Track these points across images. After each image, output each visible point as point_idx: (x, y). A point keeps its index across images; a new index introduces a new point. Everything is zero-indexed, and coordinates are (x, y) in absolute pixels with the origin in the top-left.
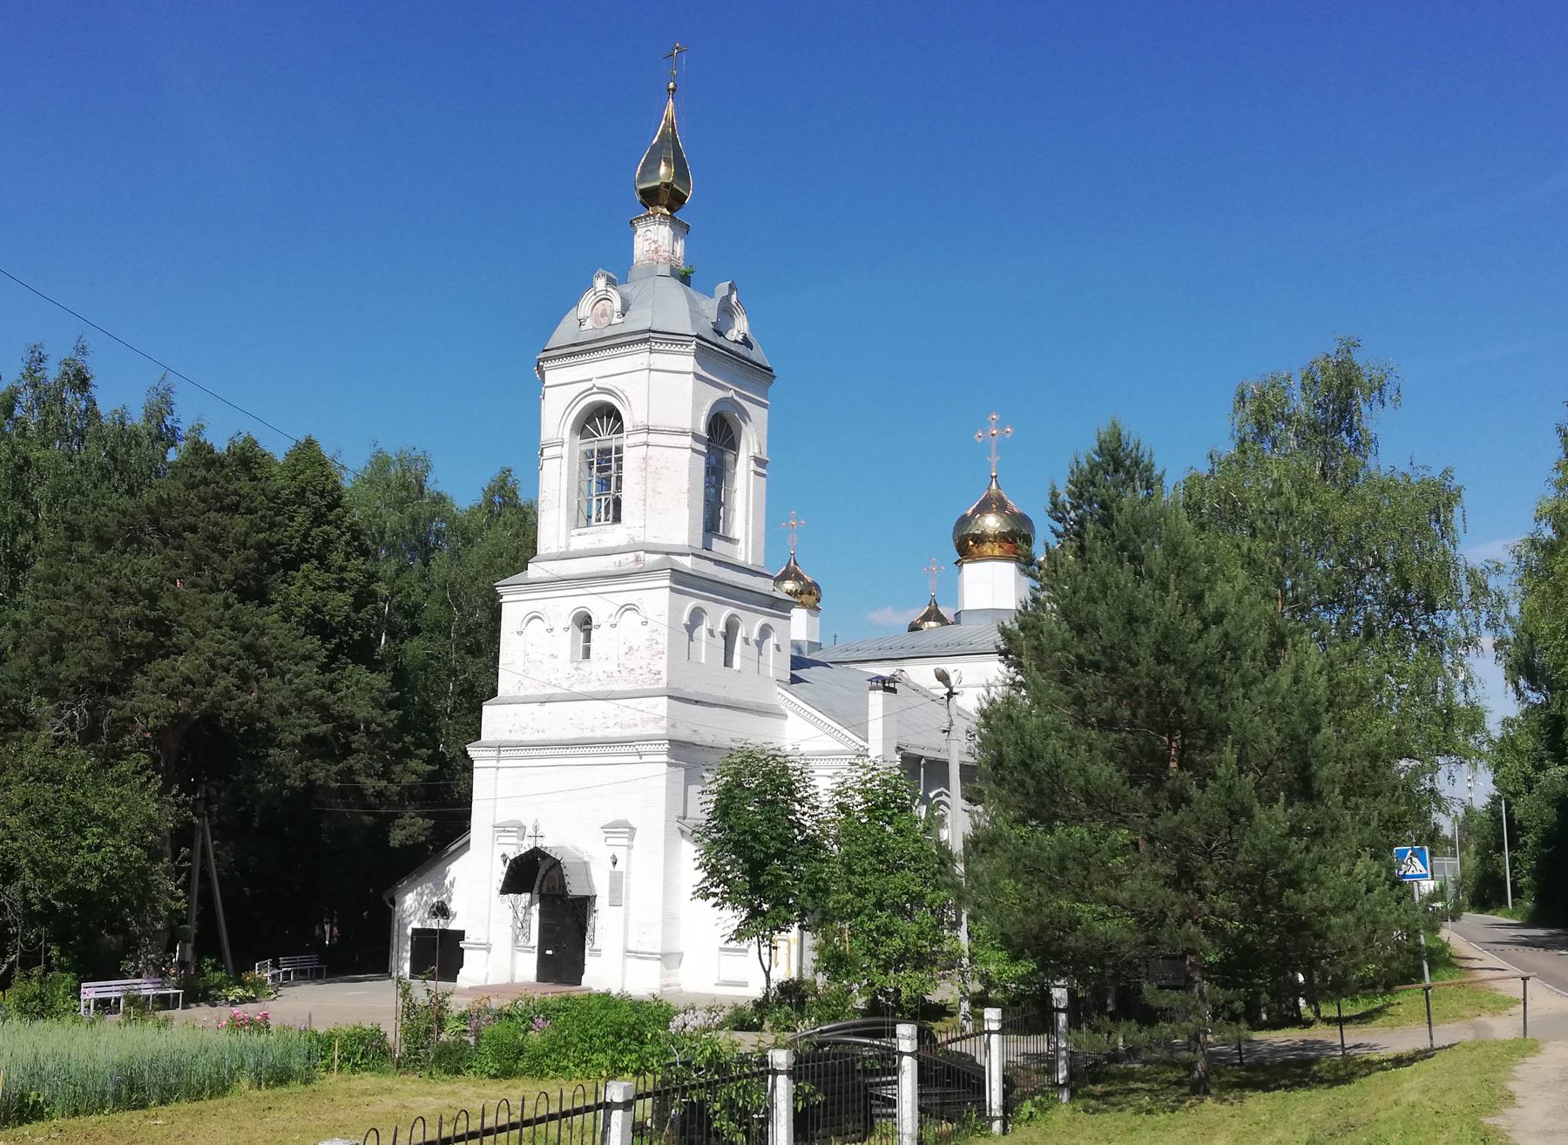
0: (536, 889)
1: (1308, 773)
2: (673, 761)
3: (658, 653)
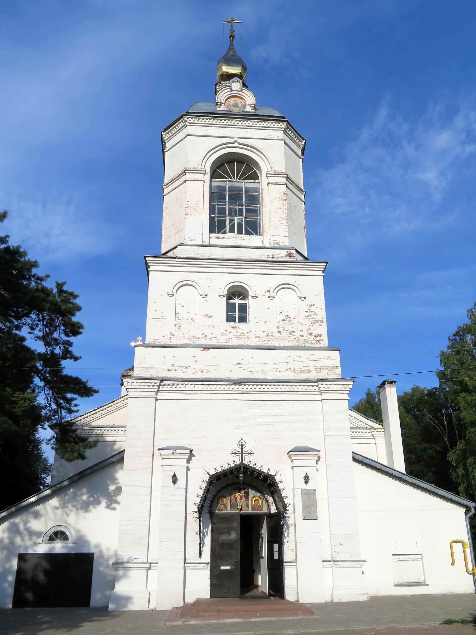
2: (444, 436)
3: (317, 321)
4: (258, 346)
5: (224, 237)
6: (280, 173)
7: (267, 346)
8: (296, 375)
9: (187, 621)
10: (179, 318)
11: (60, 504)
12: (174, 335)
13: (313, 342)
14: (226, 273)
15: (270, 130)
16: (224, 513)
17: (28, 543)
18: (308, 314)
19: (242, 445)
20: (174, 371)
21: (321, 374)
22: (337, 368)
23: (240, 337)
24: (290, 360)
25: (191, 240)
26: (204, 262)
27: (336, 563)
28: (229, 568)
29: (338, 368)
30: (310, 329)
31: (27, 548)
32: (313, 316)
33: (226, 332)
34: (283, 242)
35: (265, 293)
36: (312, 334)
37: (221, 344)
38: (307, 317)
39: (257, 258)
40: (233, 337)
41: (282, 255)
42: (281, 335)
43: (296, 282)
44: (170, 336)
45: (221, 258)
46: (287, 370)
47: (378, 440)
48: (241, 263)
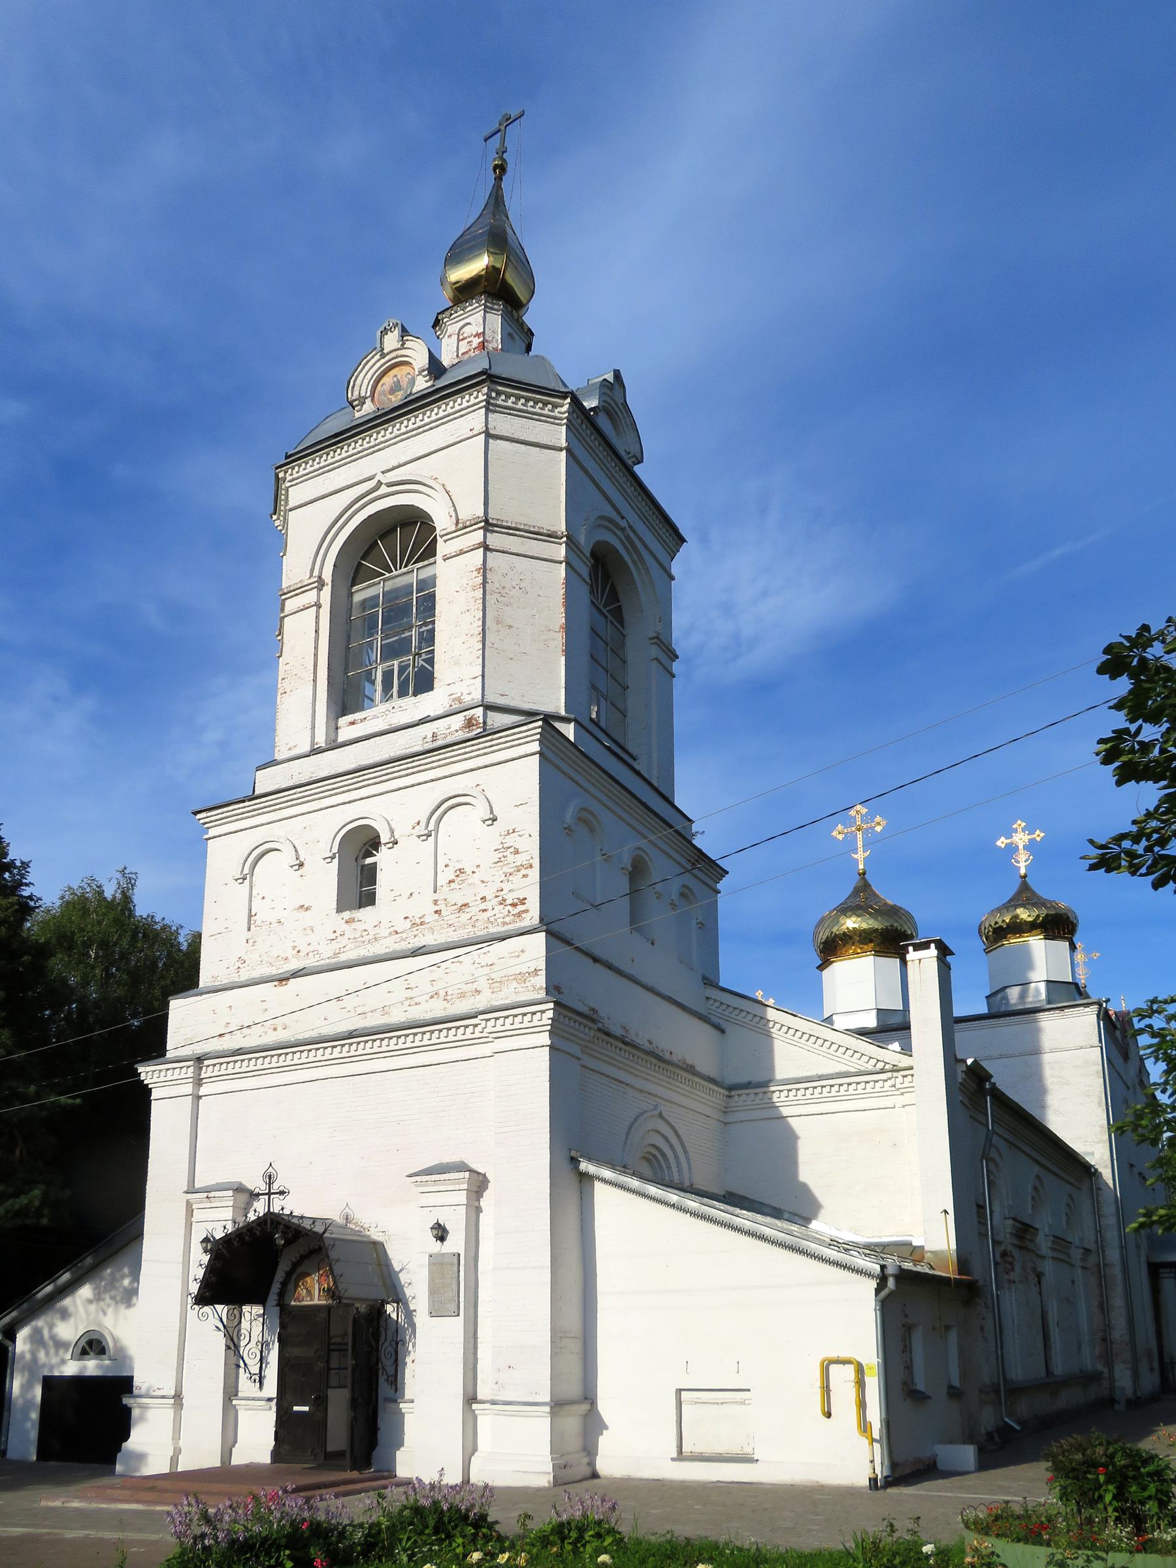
0: (272, 1298)
4: (395, 952)
5: (365, 719)
7: (390, 953)
8: (448, 1006)
9: (68, 1502)
10: (256, 924)
11: (95, 1295)
13: (507, 919)
14: (339, 805)
15: (455, 419)
17: (54, 1360)
18: (501, 855)
19: (270, 1177)
21: (502, 995)
23: (361, 939)
25: (290, 749)
26: (295, 794)
28: (306, 1409)
29: (539, 973)
30: (502, 890)
31: (52, 1368)
32: (511, 858)
34: (469, 694)
38: (496, 863)
39: (401, 752)
43: (478, 785)
44: (238, 964)
45: (333, 772)
46: (432, 997)
48: (364, 775)
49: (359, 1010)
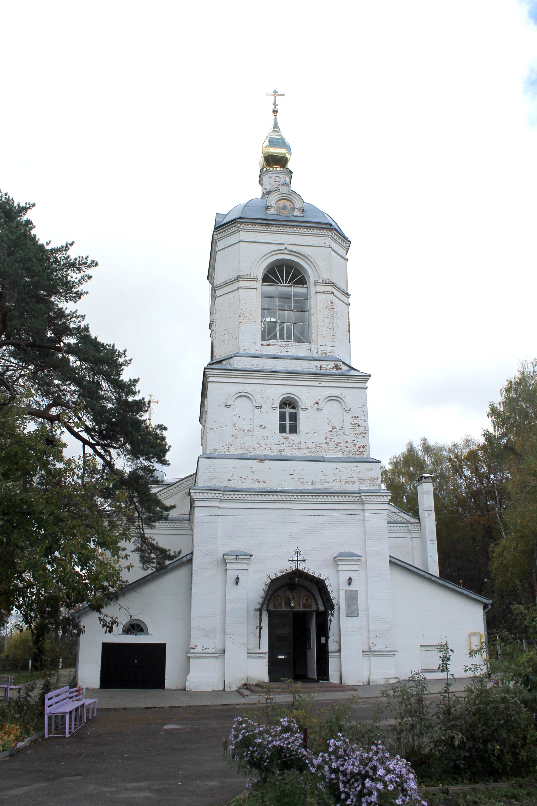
1: (4, 523)
6: (328, 282)
8: (342, 486)
12: (232, 446)
16: (279, 611)
18: (353, 426)
19: (298, 554)
20: (233, 481)
21: (364, 485)
22: (378, 480)
23: (292, 447)
24: (337, 471)
27: (373, 653)
32: (357, 428)
33: (278, 443)
35: (314, 404)
36: (356, 445)
37: (274, 454)
40: (286, 447)
41: (330, 367)
42: (328, 446)
45: (274, 369)
46: (334, 481)
47: (414, 535)
49: (301, 480)
